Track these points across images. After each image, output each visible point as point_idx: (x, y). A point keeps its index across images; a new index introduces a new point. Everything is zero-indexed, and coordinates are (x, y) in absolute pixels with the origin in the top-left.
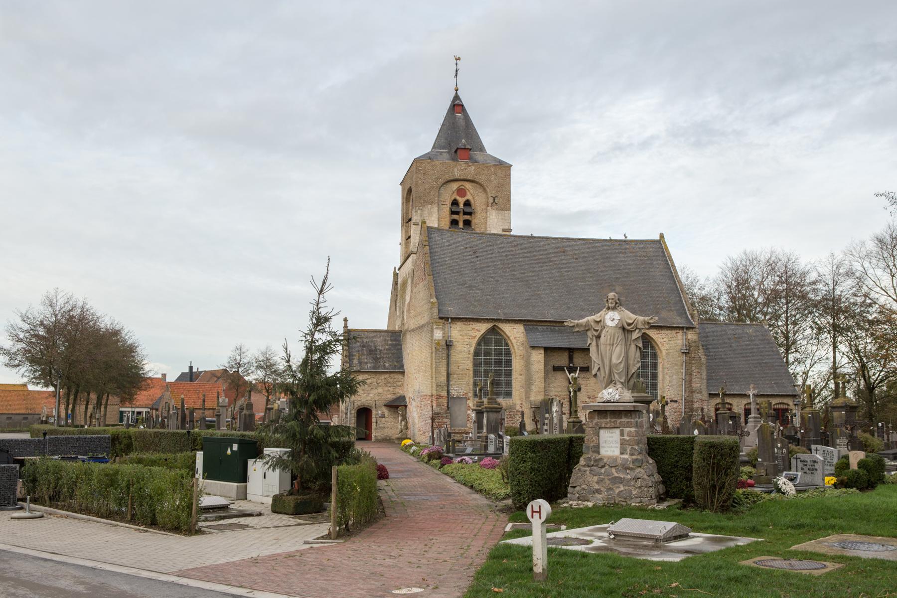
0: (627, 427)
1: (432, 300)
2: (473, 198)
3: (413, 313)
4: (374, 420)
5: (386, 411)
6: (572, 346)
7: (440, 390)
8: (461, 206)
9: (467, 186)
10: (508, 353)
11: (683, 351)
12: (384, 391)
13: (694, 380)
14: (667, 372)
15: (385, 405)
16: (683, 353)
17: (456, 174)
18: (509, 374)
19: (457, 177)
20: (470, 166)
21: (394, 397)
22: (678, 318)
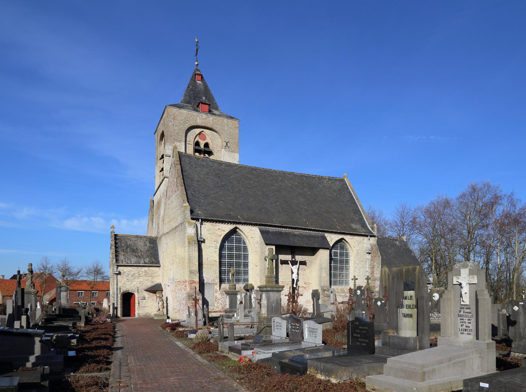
1: (184, 205)
2: (212, 141)
3: (166, 220)
4: (136, 301)
5: (146, 294)
7: (193, 277)
9: (207, 133)
11: (367, 252)
13: (375, 272)
14: (357, 266)
16: (367, 253)
17: (199, 121)
18: (246, 265)
20: (209, 117)
21: (153, 284)
22: (363, 229)
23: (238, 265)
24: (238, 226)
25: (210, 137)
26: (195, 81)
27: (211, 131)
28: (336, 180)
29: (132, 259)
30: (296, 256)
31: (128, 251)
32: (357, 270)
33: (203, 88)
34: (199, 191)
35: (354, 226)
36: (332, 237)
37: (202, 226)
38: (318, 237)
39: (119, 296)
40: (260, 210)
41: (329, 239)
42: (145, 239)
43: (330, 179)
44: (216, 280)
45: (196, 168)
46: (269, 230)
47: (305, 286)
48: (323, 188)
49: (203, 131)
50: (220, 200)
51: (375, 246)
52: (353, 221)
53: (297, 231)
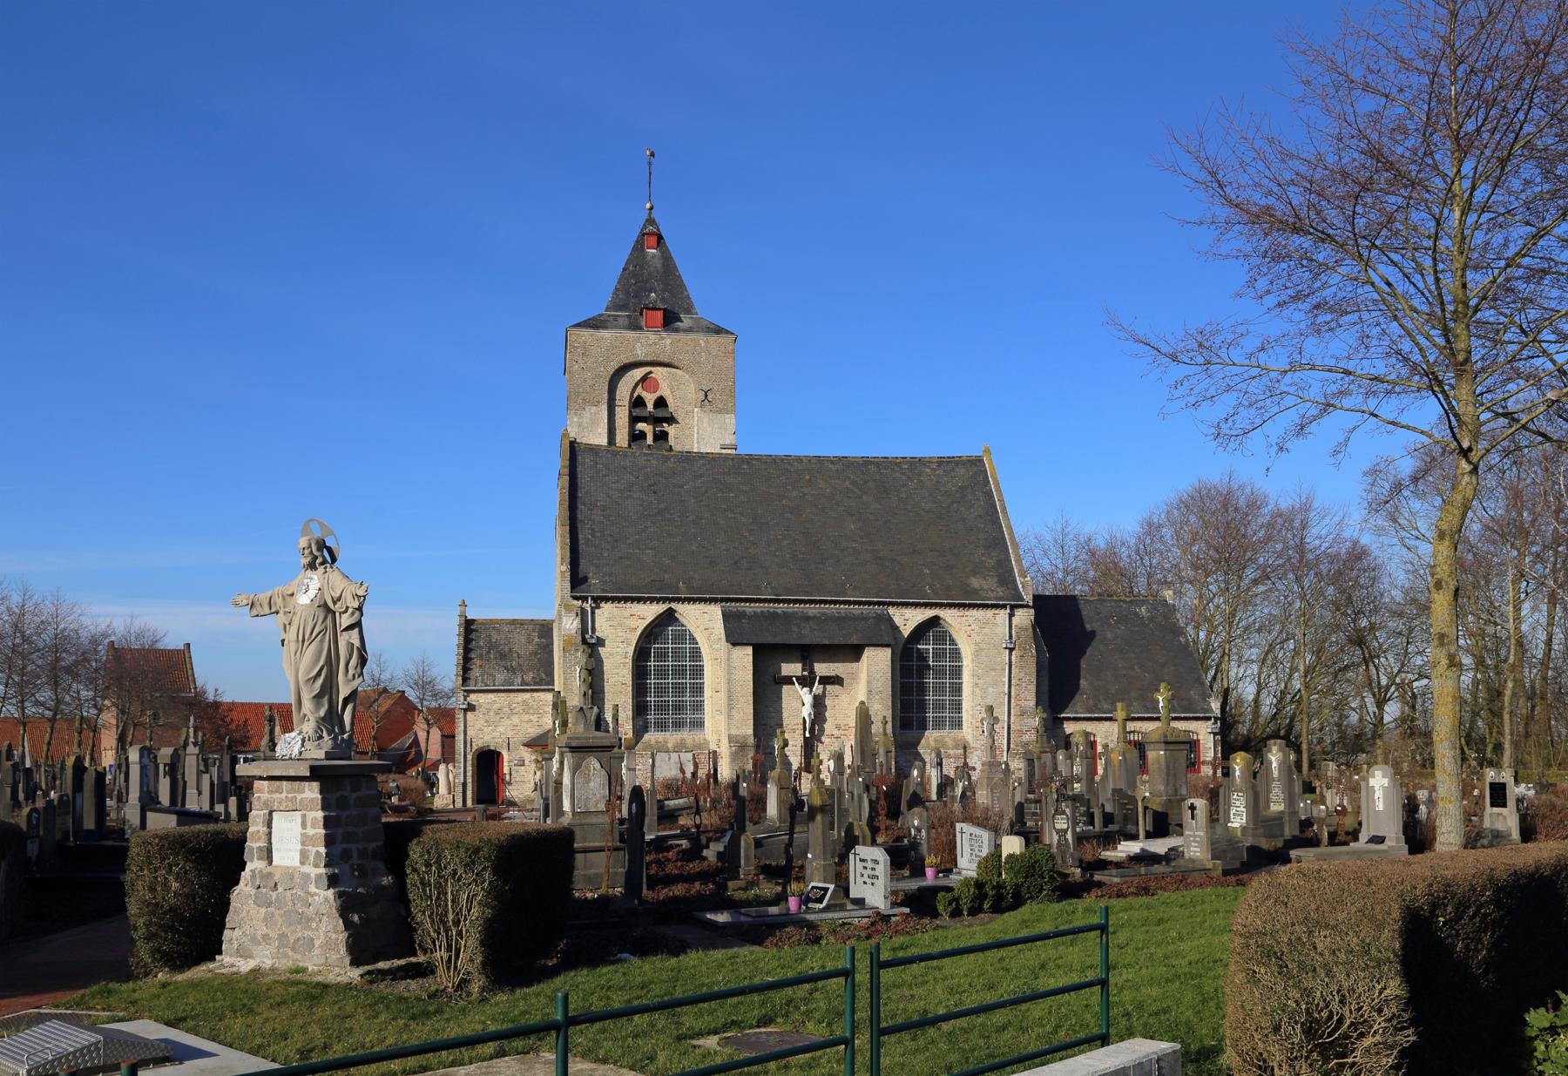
0: (311, 810)
6: (808, 642)
8: (650, 407)
10: (696, 654)
12: (522, 721)
15: (524, 745)
17: (639, 352)
18: (698, 690)
19: (641, 358)
20: (663, 339)
21: (540, 731)
23: (678, 688)
24: (673, 605)
25: (666, 383)
26: (643, 250)
27: (665, 369)
28: (957, 463)
29: (498, 676)
30: (815, 664)
31: (492, 656)
32: (977, 690)
33: (659, 266)
34: (602, 532)
35: (975, 582)
36: (907, 616)
37: (597, 611)
38: (866, 619)
39: (469, 757)
40: (736, 563)
41: (898, 620)
42: (531, 627)
43: (941, 461)
44: (485, 729)
45: (605, 476)
46: (744, 611)
47: (836, 732)
48: (916, 489)
49: (651, 372)
50: (647, 548)
51: (1026, 630)
52: (977, 570)
53: (815, 608)
